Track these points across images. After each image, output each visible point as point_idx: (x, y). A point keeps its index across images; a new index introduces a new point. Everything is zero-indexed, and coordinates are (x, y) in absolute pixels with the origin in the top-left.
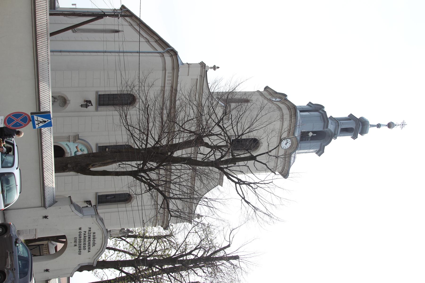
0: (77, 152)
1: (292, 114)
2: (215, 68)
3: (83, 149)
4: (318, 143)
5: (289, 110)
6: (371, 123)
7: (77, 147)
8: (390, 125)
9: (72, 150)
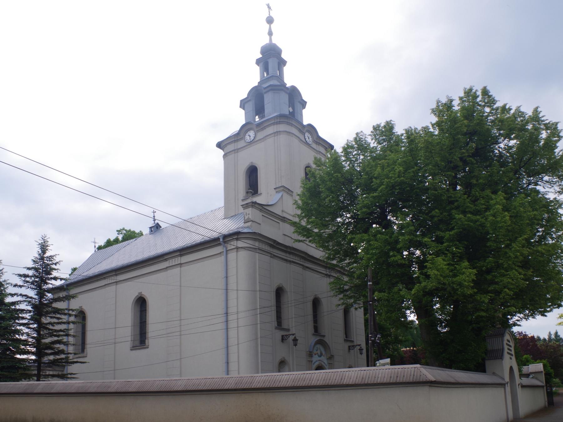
1: (286, 121)
4: (298, 106)
5: (279, 124)
6: (267, 41)
8: (270, 21)
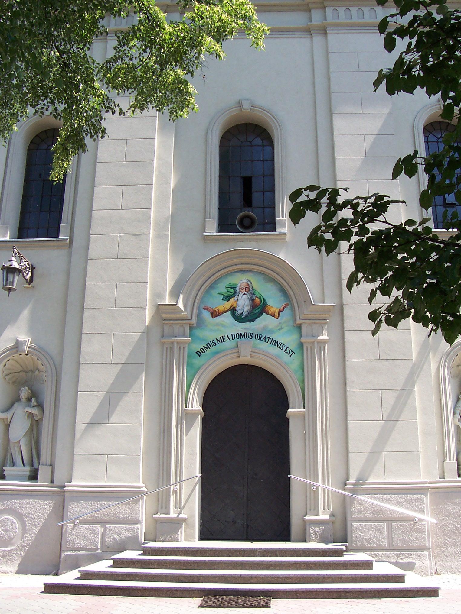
0: (239, 310)
2: (346, 190)
3: (224, 290)
7: (215, 314)
9: (228, 333)
